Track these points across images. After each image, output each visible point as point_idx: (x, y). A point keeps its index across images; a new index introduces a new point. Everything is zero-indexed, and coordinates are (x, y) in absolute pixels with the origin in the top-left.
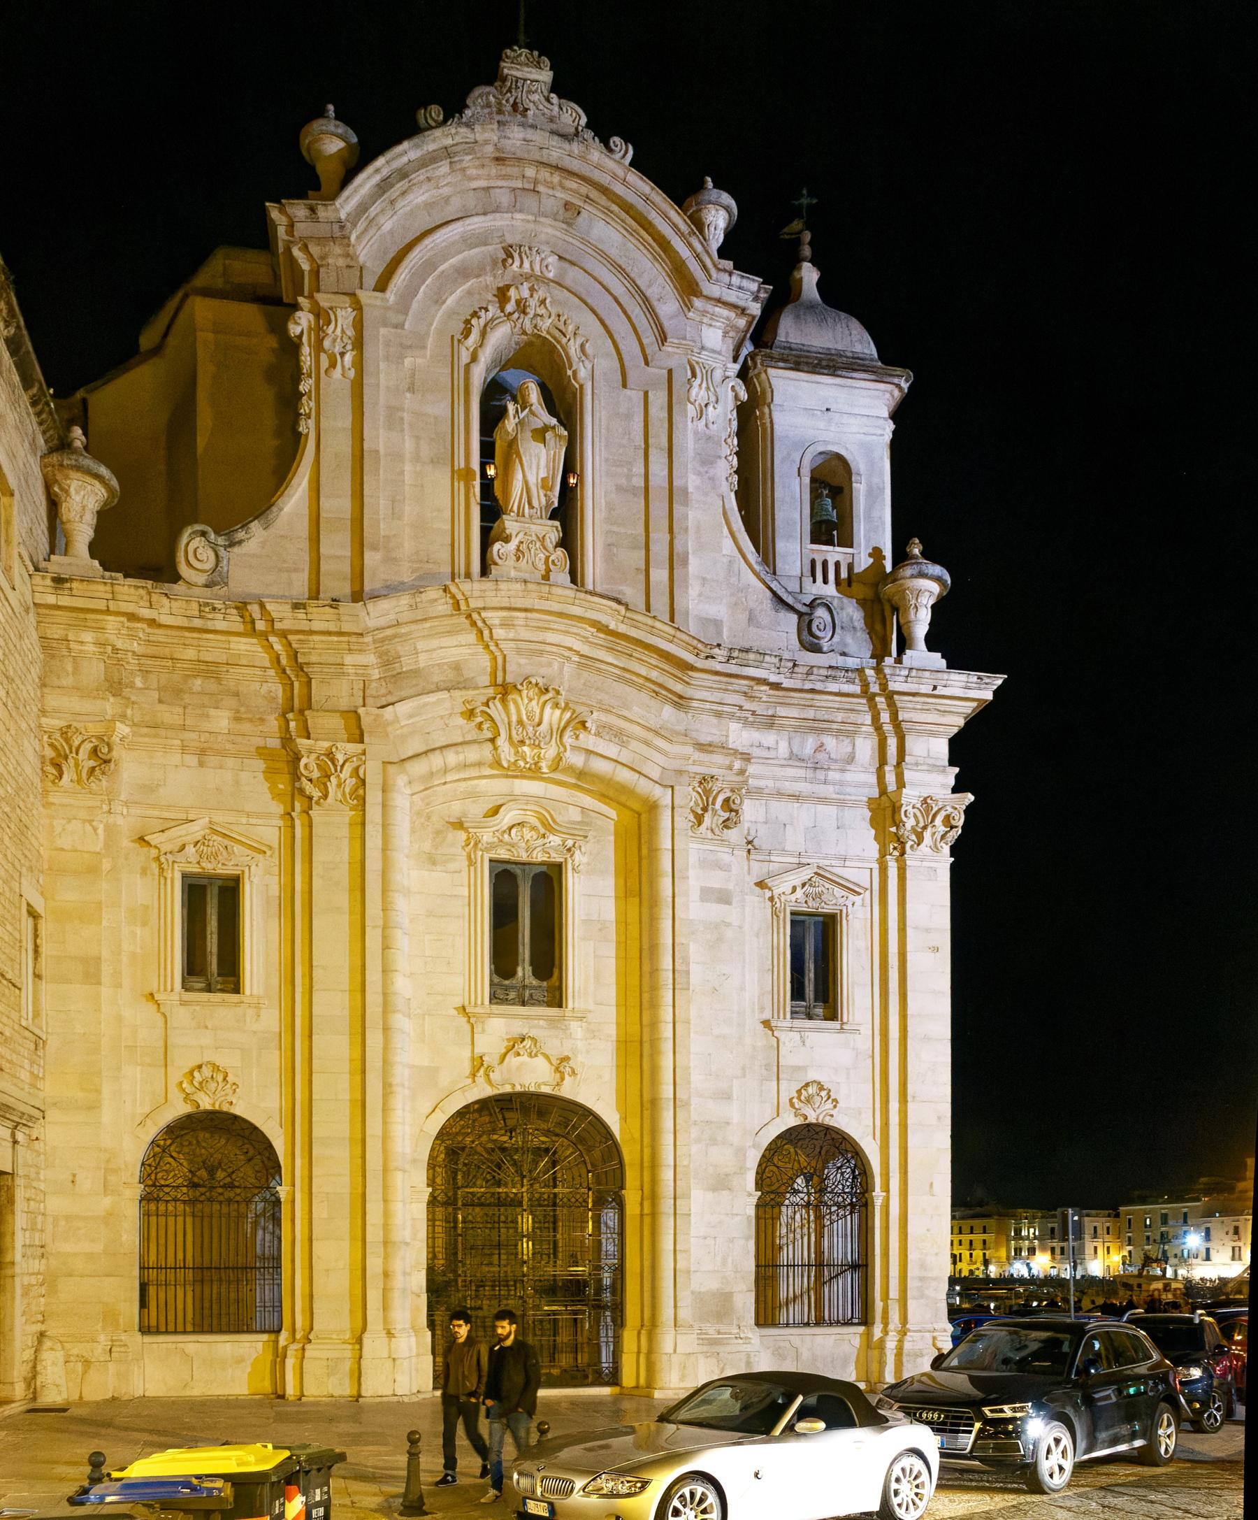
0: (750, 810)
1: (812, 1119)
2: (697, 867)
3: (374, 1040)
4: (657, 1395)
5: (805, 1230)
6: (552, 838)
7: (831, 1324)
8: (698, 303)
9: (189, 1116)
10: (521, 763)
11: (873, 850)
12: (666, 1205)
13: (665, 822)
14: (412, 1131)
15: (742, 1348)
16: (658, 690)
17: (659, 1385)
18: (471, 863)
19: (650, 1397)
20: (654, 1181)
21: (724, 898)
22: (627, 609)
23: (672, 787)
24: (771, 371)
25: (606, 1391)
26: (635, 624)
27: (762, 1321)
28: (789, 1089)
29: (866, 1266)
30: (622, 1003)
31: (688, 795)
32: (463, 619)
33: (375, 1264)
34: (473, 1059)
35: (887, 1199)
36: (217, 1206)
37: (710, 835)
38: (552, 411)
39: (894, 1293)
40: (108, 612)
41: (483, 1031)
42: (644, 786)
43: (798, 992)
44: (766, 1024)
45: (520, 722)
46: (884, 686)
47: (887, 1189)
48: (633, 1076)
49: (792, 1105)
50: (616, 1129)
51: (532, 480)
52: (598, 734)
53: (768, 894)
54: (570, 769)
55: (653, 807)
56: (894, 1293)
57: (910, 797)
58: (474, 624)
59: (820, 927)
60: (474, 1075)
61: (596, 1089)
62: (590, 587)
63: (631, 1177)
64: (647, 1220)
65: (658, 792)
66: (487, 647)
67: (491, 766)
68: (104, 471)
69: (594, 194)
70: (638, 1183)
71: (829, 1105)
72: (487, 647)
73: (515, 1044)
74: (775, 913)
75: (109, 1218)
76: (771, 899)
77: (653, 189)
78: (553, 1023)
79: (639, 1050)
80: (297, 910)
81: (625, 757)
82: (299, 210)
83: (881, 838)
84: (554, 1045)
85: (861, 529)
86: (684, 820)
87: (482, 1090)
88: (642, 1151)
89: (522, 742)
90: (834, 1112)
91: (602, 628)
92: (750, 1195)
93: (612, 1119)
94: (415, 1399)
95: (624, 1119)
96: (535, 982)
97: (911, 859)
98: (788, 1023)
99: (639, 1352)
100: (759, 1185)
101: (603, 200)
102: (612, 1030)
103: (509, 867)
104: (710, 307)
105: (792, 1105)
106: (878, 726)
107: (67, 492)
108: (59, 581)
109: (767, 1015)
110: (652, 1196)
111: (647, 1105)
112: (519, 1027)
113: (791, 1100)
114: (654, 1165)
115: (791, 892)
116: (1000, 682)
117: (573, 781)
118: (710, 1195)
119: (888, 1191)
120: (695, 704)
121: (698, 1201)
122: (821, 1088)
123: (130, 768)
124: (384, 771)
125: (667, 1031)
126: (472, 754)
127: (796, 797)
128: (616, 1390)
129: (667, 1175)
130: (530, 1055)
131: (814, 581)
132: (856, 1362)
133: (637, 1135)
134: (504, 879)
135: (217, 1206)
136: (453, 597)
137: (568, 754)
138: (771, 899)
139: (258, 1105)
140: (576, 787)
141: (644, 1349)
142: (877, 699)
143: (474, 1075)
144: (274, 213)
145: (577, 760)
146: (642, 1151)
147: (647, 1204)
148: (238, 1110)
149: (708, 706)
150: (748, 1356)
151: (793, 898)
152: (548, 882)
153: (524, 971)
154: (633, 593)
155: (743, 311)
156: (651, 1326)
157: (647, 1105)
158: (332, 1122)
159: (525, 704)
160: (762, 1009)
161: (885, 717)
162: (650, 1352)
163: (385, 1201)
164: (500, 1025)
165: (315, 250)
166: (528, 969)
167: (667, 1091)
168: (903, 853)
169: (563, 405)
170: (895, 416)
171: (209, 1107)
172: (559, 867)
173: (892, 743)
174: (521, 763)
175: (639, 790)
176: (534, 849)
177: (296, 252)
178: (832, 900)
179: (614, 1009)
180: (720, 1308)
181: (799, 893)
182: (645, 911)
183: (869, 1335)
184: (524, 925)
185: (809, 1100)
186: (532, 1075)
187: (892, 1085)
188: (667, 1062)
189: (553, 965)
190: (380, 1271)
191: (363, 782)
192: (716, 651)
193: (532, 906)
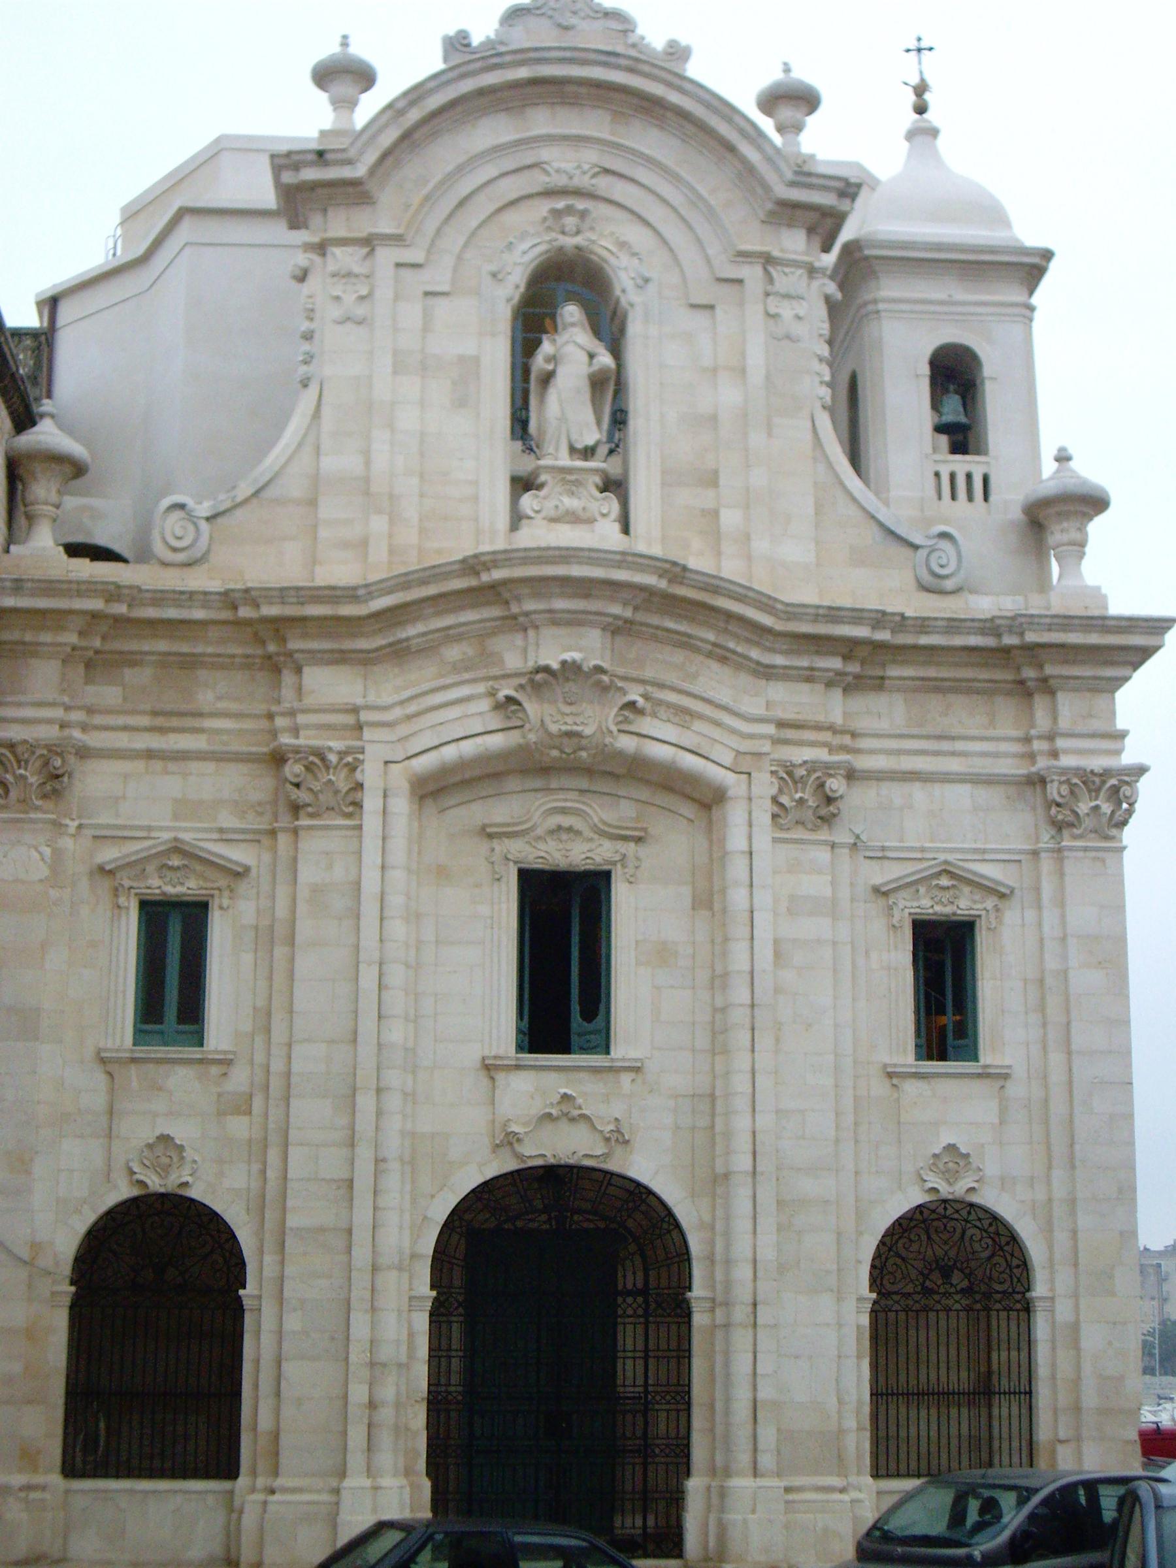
0: (859, 801)
9: (134, 1200)
14: (406, 1229)
23: (749, 774)
27: (882, 1471)
29: (1030, 1393)
36: (157, 1331)
38: (597, 332)
75: (31, 1334)
77: (860, 1429)
81: (688, 739)
100: (876, 1281)
123: (94, 781)
131: (940, 498)
135: (157, 1331)
139: (222, 1189)
169: (610, 327)
172: (606, 876)
186: (569, 1146)
189: (599, 1001)
190: (366, 1399)
193: (185, 1476)
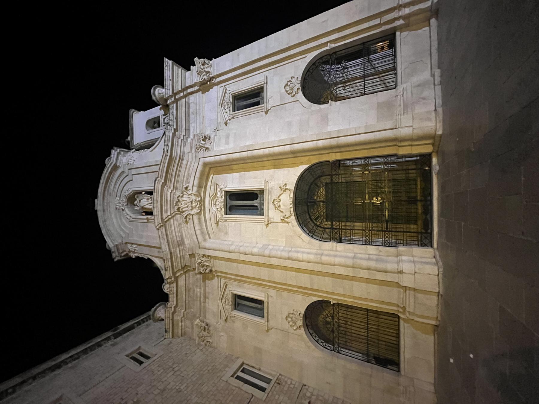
1: (299, 86)
2: (222, 148)
3: (273, 261)
4: (440, 132)
5: (354, 85)
6: (218, 195)
7: (395, 63)
8: (118, 164)
10: (198, 206)
11: (215, 88)
12: (334, 142)
13: (208, 160)
14: (307, 248)
15: (409, 91)
16: (179, 165)
17: (432, 132)
18: (226, 221)
19: (441, 136)
20: (325, 148)
21: (228, 136)
22: (158, 177)
24: (135, 144)
25: (434, 160)
26: (162, 175)
28: (289, 98)
30: (262, 168)
31: (201, 154)
32: (167, 223)
33: (363, 274)
34: (282, 222)
35: (330, 42)
37: (212, 144)
39: (377, 21)
40: (173, 319)
41: (273, 218)
42: (200, 168)
43: (258, 103)
44: (266, 113)
45: (187, 207)
46: (171, 96)
47: (326, 44)
48: (285, 161)
49: (294, 96)
50: (305, 167)
51: (147, 203)
52: (189, 183)
53: (229, 121)
54: (198, 191)
55: (205, 164)
56: (377, 21)
57: (197, 79)
58: (168, 220)
59: (239, 101)
60: (288, 222)
61: (291, 176)
62: (153, 188)
63: (324, 158)
64: (342, 149)
65: (201, 163)
66: (174, 216)
67: (200, 215)
68: (157, 305)
69: (107, 190)
70: (327, 155)
71: (293, 80)
72: (174, 216)
73: (277, 208)
74: (233, 118)
76: (230, 120)
78: (269, 193)
79: (276, 160)
80: (241, 279)
82: (114, 255)
83: (211, 87)
84: (276, 192)
85: (156, 115)
86: (207, 154)
87: (293, 219)
88: (313, 155)
89: (192, 206)
90: (296, 77)
91: (164, 184)
92: (331, 105)
93: (301, 169)
94: (440, 263)
95: (301, 164)
96: (259, 199)
97: (214, 74)
98: (265, 105)
99: (411, 145)
101: (107, 188)
102: (271, 171)
103: (228, 207)
104: (119, 161)
105: (294, 96)
106: (185, 96)
107: (160, 317)
108: (166, 331)
109: (264, 113)
110: (331, 148)
111: (295, 155)
112: (271, 206)
113: (292, 97)
114: (317, 149)
115: (228, 112)
116: (167, 59)
117: (203, 189)
118: (330, 123)
119: (327, 42)
120: (182, 154)
121: (332, 128)
122: (287, 85)
124: (201, 248)
125: (267, 151)
126: (196, 221)
127: (204, 117)
128: (434, 155)
129: (320, 143)
130: (280, 202)
132: (417, 30)
133: (307, 158)
134: (230, 210)
136: (160, 227)
137: (193, 192)
138: (230, 120)
139: (301, 304)
140: (205, 188)
141: (410, 143)
142: (177, 97)
143: (288, 222)
144: (116, 260)
145: (195, 189)
146: (313, 155)
147: (335, 150)
148: (303, 311)
149: (182, 150)
150: (415, 87)
151: (228, 112)
152: (232, 195)
153: (255, 203)
154: (154, 175)
155: (119, 154)
156: (396, 141)
157: (295, 155)
158: (304, 280)
159: (183, 205)
160: (262, 116)
161: (182, 94)
162: (412, 140)
163: (334, 265)
164: (272, 213)
165: (121, 251)
166: (255, 201)
167: (287, 148)
168: (213, 77)
170: (140, 110)
171: (302, 322)
173: (190, 90)
174: (198, 206)
175: (201, 169)
176: (221, 200)
177: (123, 255)
178: (229, 98)
179: (265, 171)
180: (386, 108)
181: (227, 110)
182: (234, 163)
183: (401, 28)
184: (245, 202)
185: (292, 89)
187: (283, 56)
188: (277, 150)
191: (204, 255)
192: (165, 150)
